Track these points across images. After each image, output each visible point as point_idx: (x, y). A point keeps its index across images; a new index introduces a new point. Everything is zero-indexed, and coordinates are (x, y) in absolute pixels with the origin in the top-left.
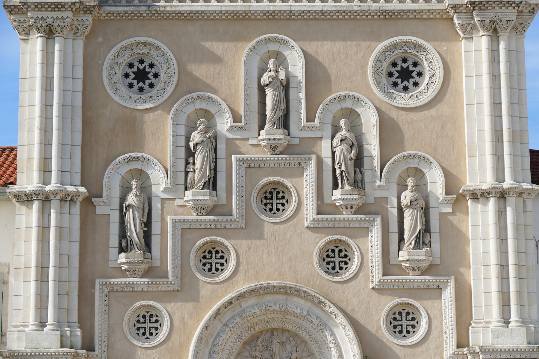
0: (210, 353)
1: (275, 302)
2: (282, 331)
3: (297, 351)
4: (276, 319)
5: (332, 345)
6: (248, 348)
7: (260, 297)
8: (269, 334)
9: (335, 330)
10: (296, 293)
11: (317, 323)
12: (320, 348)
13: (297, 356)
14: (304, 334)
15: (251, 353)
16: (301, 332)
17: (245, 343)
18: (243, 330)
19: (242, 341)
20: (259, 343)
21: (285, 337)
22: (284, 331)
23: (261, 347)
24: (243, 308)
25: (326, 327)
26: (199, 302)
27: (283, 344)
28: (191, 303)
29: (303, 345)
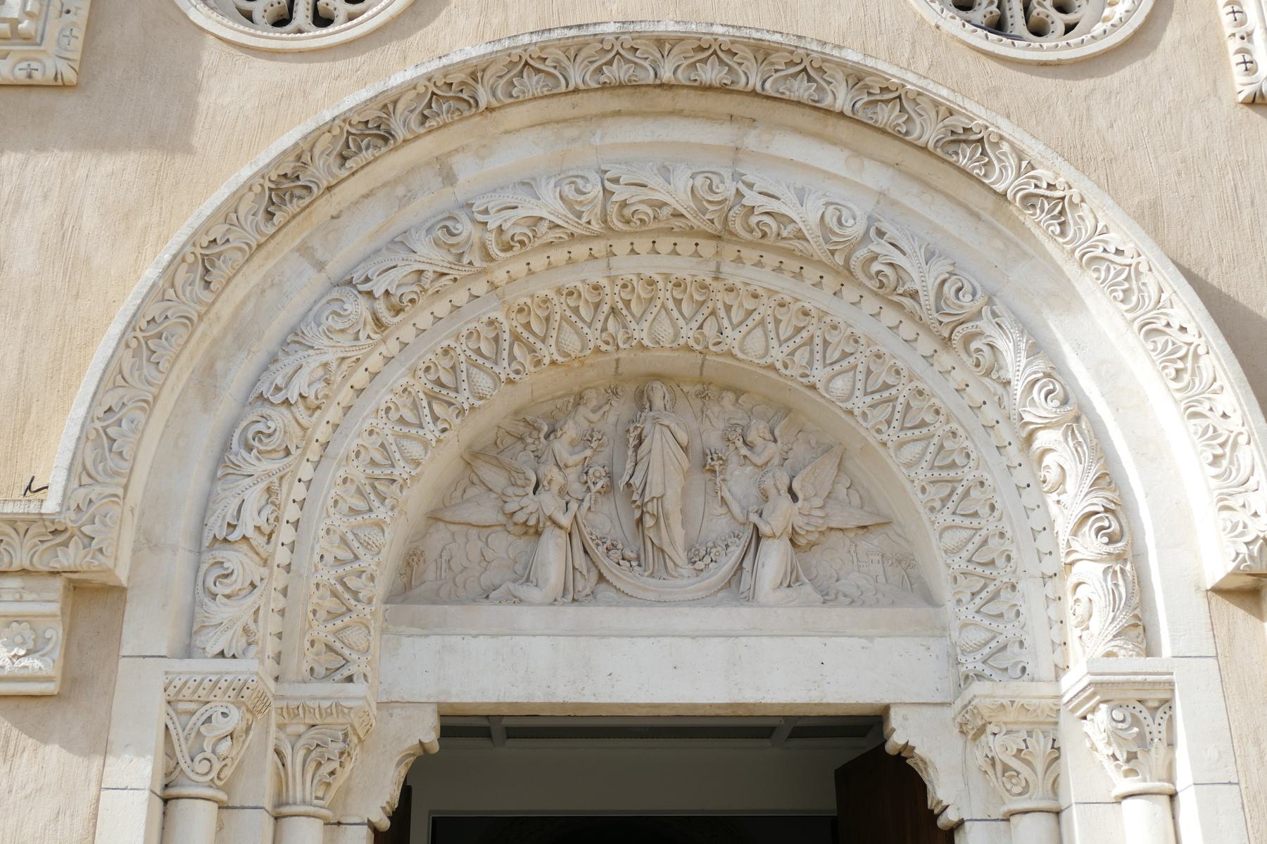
0: (226, 447)
1: (669, 158)
2: (702, 396)
3: (795, 498)
4: (665, 294)
5: (1039, 410)
6: (495, 477)
7: (571, 132)
8: (621, 409)
9: (1059, 329)
10: (801, 89)
11: (932, 284)
12: (946, 465)
13: (799, 522)
14: (840, 385)
15: (511, 507)
16: (819, 374)
17: (473, 456)
18: (463, 350)
19: (462, 434)
20: (560, 447)
21: (721, 425)
22: (709, 387)
23: (572, 474)
24: (461, 191)
25: (990, 302)
26: (188, 150)
27: (708, 465)
28: (133, 156)
29: (828, 467)
